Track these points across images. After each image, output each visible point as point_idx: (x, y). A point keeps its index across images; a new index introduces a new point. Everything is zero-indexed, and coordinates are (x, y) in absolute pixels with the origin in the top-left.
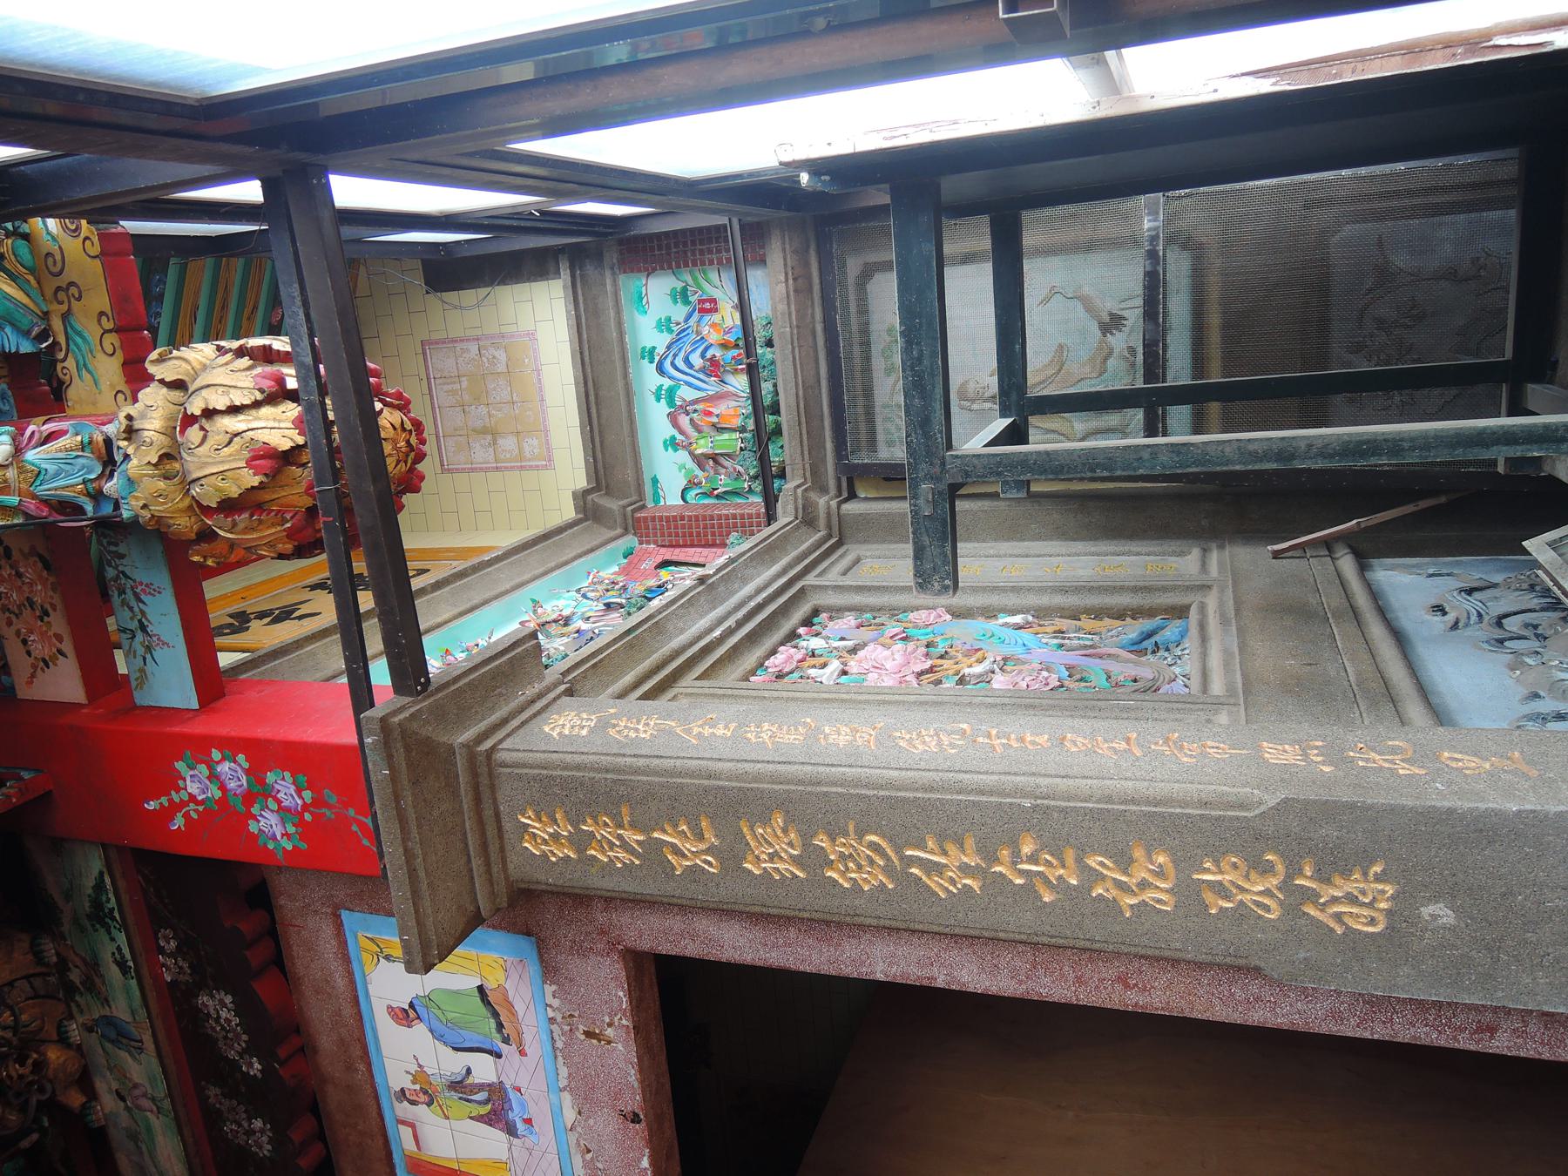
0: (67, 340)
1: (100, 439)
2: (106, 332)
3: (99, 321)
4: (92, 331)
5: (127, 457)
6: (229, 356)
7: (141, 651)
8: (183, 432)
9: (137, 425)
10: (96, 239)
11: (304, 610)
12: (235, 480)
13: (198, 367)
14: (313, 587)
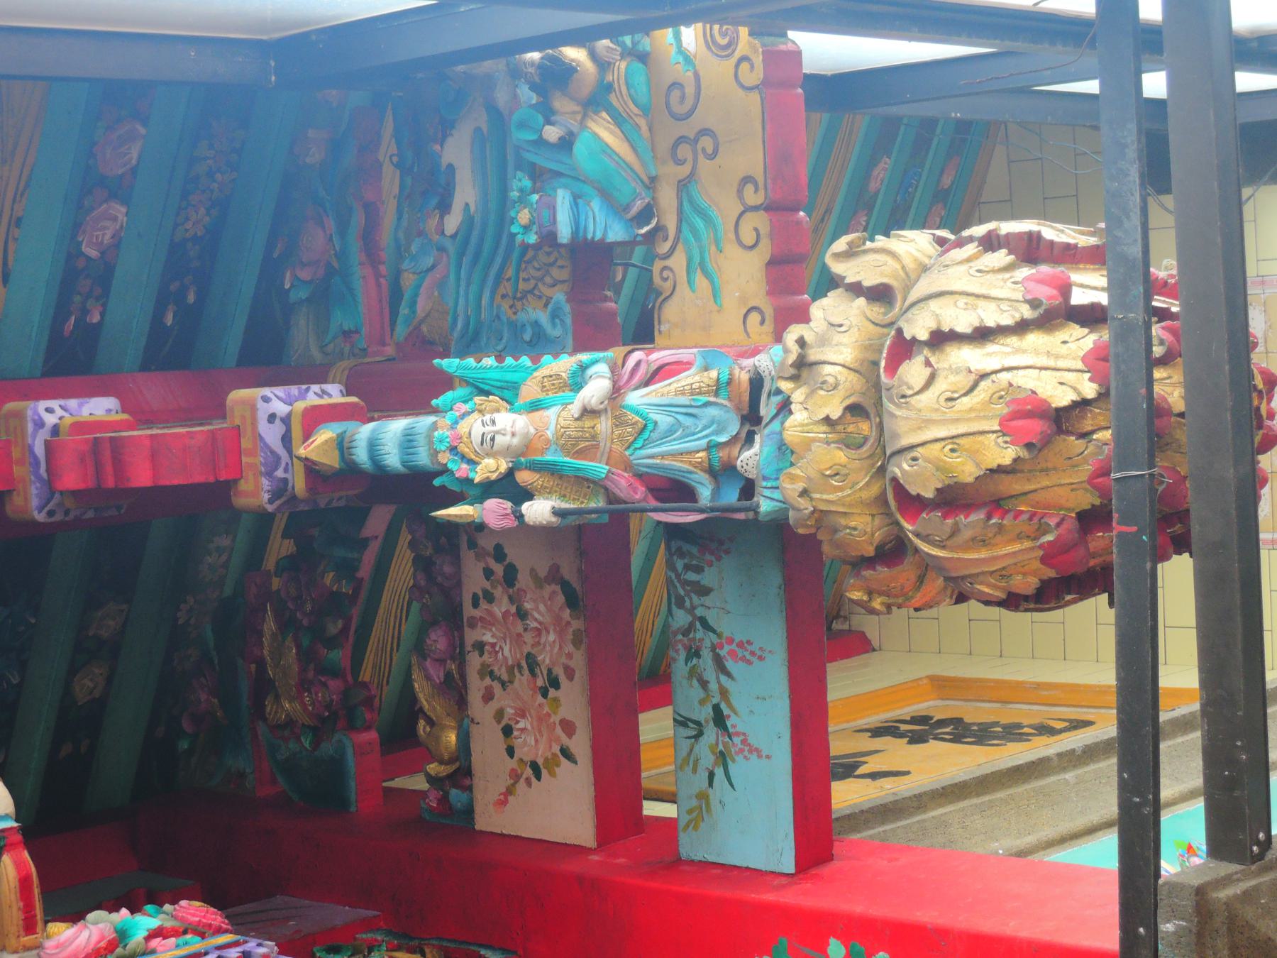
0: (680, 221)
1: (745, 377)
2: (749, 209)
3: (740, 192)
4: (725, 206)
5: (785, 407)
6: (971, 249)
7: (707, 760)
8: (893, 367)
9: (813, 355)
10: (758, 60)
11: (872, 765)
12: (973, 454)
13: (911, 265)
14: (877, 732)
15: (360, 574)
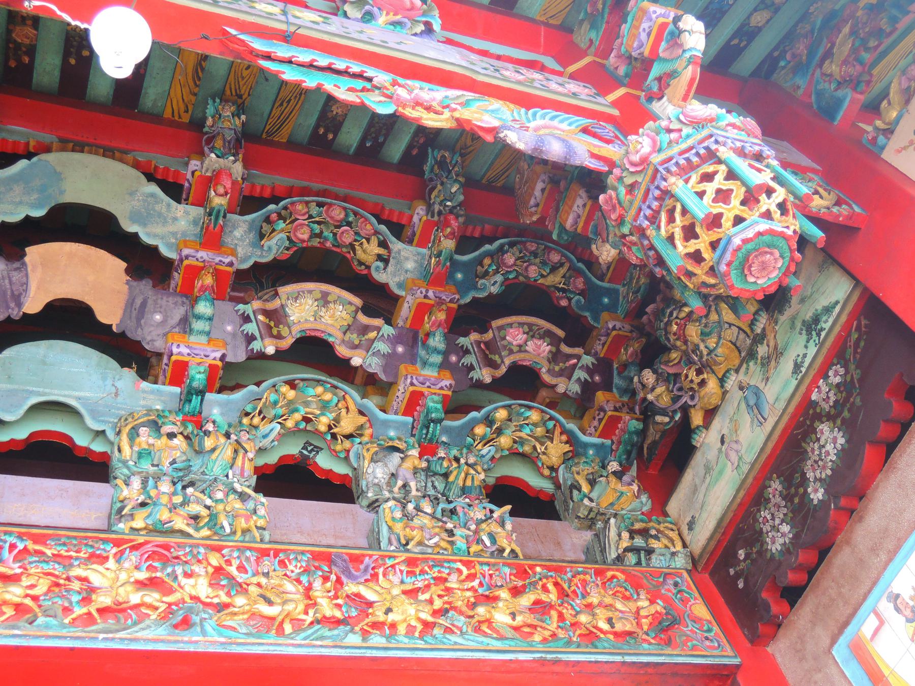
15: (897, 26)
